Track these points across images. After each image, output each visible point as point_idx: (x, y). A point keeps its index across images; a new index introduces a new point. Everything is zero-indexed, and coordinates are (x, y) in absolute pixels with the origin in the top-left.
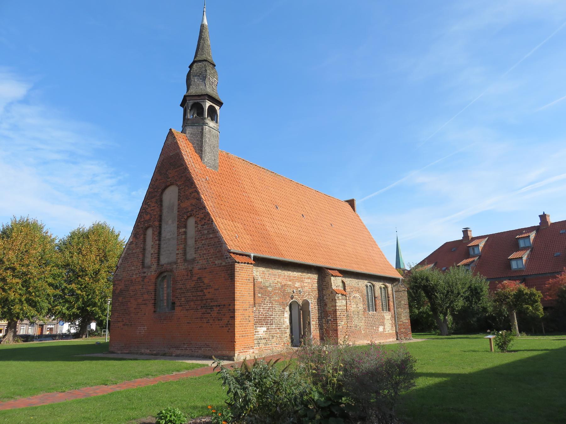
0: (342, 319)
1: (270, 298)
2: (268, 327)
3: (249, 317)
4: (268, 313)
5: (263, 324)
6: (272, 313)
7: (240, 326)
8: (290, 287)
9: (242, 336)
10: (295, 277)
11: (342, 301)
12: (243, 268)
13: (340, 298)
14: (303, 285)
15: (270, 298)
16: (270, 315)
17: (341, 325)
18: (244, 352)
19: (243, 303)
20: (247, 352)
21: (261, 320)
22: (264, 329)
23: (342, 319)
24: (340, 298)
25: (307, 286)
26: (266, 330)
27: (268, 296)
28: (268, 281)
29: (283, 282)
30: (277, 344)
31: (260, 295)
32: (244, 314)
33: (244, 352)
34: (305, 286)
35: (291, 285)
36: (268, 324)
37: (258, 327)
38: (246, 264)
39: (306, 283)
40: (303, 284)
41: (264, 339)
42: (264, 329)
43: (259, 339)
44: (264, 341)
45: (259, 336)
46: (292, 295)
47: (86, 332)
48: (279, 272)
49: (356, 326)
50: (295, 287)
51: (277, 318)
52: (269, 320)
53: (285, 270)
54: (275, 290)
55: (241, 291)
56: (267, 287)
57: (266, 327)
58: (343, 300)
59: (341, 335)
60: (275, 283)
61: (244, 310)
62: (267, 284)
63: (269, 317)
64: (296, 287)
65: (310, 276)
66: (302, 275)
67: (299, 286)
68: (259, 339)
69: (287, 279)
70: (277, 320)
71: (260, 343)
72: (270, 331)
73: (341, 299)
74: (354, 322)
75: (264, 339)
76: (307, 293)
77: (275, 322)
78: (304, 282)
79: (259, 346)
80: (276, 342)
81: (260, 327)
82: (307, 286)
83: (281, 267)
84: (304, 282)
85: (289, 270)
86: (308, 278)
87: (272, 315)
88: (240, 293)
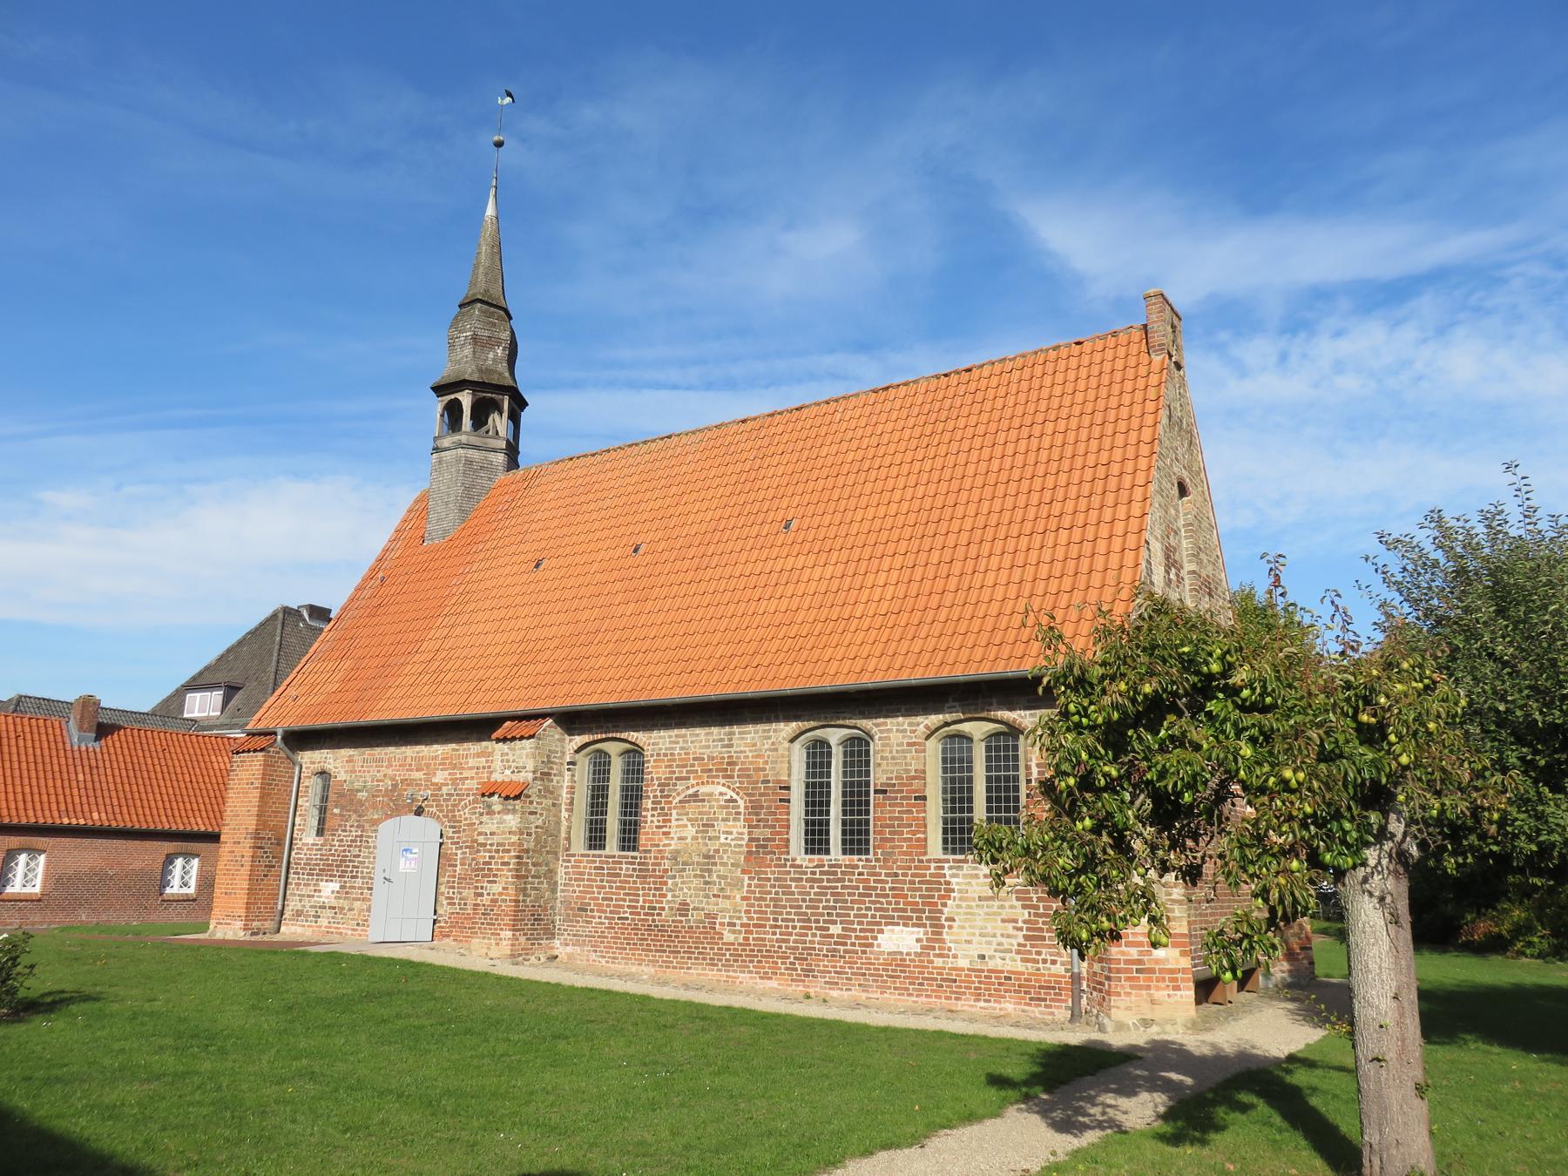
0: (495, 875)
1: (360, 816)
2: (345, 882)
3: (243, 856)
4: (349, 851)
5: (335, 876)
6: (360, 851)
7: (225, 875)
8: (417, 785)
9: (226, 893)
10: (436, 758)
11: (505, 817)
12: (244, 761)
13: (497, 808)
14: (458, 776)
15: (360, 816)
16: (355, 856)
17: (488, 894)
18: (226, 924)
19: (234, 829)
20: (229, 924)
21: (332, 865)
22: (335, 886)
23: (495, 875)
24: (497, 808)
25: (472, 778)
26: (337, 889)
27: (355, 811)
28: (361, 777)
29: (400, 775)
30: (358, 924)
31: (336, 811)
32: (234, 852)
33: (226, 924)
34: (467, 778)
35: (421, 780)
36: (344, 877)
37: (322, 880)
38: (252, 753)
39: (471, 768)
40: (461, 774)
41: (330, 908)
42: (335, 886)
43: (320, 907)
44: (330, 913)
45: (322, 900)
46: (420, 807)
47: (1485, 935)
48: (379, 752)
49: (683, 909)
50: (432, 784)
51: (369, 862)
52: (348, 866)
53: (406, 743)
54: (373, 796)
55: (235, 807)
56: (358, 791)
57: (340, 882)
58: (508, 814)
59: (483, 924)
60: (377, 781)
61: (235, 843)
62: (357, 785)
63: (350, 861)
64: (437, 784)
65: (487, 748)
66: (457, 750)
67: (446, 779)
68: (320, 907)
69: (410, 765)
70: (368, 868)
71: (319, 917)
72: (347, 893)
73: (499, 813)
74: (669, 894)
75: (330, 908)
76: (471, 798)
77: (362, 872)
78: (463, 768)
79: (316, 922)
80: (357, 920)
81: (327, 881)
82: (472, 778)
83: (397, 738)
84: (463, 768)
85: (417, 743)
86: (478, 755)
87: (359, 856)
88: (232, 811)
